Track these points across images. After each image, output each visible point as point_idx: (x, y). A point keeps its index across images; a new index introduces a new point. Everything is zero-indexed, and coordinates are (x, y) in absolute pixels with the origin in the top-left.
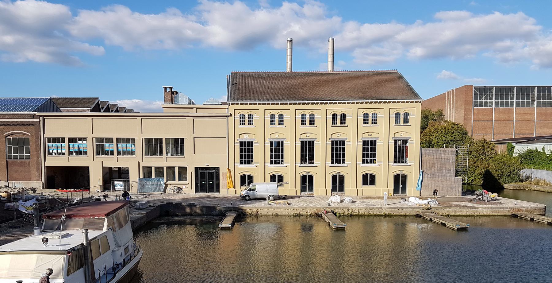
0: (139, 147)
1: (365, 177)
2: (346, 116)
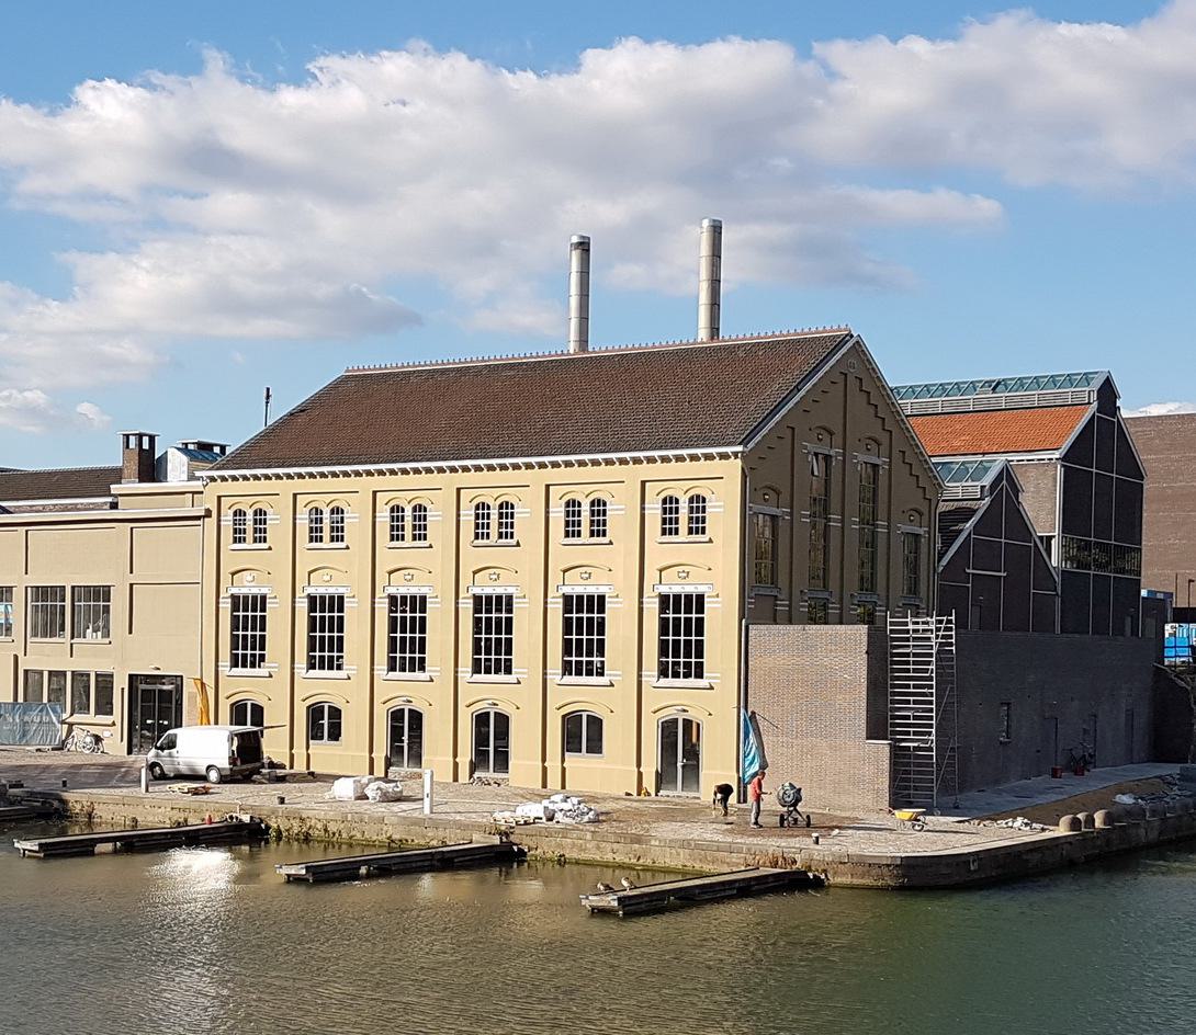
1: (571, 723)
2: (707, 504)
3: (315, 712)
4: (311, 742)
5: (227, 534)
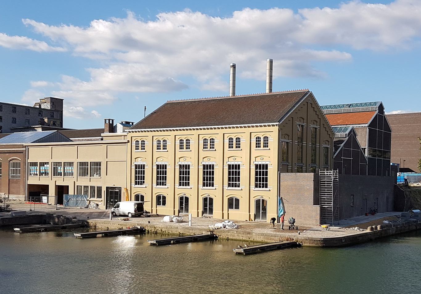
0: (75, 169)
1: (230, 201)
2: (269, 139)
3: (158, 197)
4: (229, 209)
5: (134, 147)
